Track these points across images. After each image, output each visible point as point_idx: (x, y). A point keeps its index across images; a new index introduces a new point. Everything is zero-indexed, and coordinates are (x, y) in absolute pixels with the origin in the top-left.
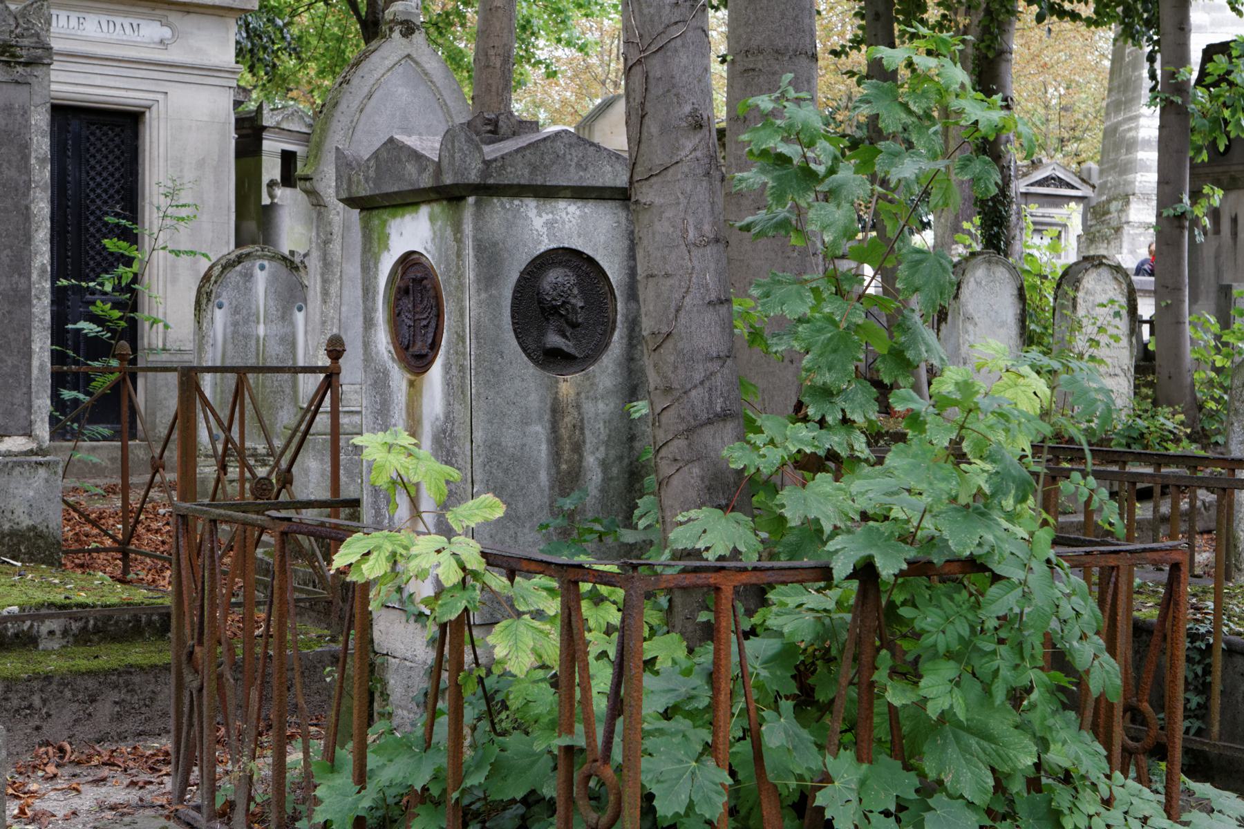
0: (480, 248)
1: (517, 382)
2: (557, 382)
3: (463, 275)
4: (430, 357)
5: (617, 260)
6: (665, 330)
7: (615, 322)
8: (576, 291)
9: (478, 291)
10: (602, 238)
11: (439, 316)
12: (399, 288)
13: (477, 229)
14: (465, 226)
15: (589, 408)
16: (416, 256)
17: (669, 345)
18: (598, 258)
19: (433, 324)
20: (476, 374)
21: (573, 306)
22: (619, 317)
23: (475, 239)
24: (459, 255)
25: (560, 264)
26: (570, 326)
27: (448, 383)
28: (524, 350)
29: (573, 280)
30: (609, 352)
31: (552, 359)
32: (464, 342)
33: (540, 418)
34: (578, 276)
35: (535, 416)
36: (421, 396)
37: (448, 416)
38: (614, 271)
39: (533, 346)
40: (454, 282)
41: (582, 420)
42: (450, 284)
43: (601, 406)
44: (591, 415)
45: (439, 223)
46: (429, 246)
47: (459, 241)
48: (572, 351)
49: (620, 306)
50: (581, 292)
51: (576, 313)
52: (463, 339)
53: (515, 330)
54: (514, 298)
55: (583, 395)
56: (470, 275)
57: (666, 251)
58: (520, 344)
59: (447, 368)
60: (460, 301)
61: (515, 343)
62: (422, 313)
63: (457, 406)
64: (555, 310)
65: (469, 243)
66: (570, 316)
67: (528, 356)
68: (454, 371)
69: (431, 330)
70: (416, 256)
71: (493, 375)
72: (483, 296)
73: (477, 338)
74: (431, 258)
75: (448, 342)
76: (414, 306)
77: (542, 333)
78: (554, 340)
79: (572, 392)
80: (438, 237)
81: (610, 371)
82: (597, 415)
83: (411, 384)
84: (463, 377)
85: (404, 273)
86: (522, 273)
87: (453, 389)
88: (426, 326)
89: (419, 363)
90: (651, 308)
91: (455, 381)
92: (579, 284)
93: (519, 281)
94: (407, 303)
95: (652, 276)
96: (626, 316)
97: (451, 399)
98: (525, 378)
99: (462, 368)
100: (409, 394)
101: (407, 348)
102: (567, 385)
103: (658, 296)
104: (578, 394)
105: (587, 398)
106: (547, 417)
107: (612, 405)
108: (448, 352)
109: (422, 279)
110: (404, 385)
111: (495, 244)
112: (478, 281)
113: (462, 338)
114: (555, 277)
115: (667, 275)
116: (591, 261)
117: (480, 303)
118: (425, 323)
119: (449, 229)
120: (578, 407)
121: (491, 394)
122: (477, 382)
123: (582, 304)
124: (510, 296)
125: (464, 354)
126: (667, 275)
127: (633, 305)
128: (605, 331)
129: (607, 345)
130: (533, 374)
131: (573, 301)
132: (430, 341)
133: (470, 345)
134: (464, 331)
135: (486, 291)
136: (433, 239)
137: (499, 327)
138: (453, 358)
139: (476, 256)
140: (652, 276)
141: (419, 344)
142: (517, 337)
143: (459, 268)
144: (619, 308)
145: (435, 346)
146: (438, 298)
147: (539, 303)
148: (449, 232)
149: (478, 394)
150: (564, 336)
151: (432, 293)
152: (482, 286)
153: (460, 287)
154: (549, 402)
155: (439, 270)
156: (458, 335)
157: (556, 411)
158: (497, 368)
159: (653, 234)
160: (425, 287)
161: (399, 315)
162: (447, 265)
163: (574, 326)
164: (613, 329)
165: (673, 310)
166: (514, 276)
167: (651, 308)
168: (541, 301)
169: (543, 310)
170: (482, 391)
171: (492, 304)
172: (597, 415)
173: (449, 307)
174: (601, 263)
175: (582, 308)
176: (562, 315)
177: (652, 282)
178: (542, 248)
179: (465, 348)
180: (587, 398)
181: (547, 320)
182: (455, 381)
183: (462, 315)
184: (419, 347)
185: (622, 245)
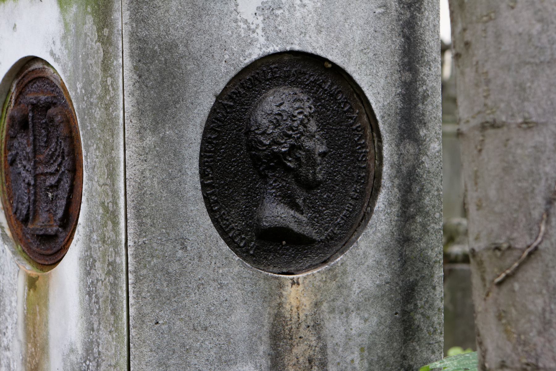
0: (143, 54)
1: (212, 291)
2: (281, 286)
3: (112, 102)
4: (61, 240)
5: (382, 71)
6: (522, 241)
7: (378, 176)
8: (313, 127)
9: (141, 133)
10: (358, 34)
11: (75, 170)
12: (12, 118)
13: (138, 19)
14: (117, 15)
15: (335, 328)
16: (37, 65)
17: (533, 273)
18: (350, 69)
19: (66, 185)
20: (138, 280)
21: (309, 153)
22: (386, 168)
23: (135, 38)
24: (106, 67)
25: (287, 80)
26: (300, 186)
27: (90, 291)
28: (223, 232)
29: (308, 106)
30: (369, 230)
31: (271, 248)
32: (116, 224)
33: (252, 351)
34: (317, 100)
35: (242, 348)
36: (46, 306)
37: (89, 347)
38: (378, 89)
39: (238, 225)
40: (98, 113)
41: (323, 350)
42: (92, 117)
43: (356, 322)
44: (339, 339)
45: (74, 9)
46: (58, 48)
47: (106, 41)
48: (307, 230)
49: (387, 150)
50: (322, 126)
51: (314, 165)
52: (113, 216)
53: (206, 198)
54: (206, 141)
55: (325, 306)
56: (125, 102)
57: (526, 72)
58: (215, 222)
59: (88, 265)
60: (108, 148)
61: (207, 221)
62: (48, 163)
63: (104, 335)
64: (278, 159)
65: (123, 45)
66: (303, 170)
67: (230, 242)
68: (99, 272)
69: (63, 193)
70: (37, 65)
71: (164, 279)
72: (150, 140)
73: (138, 216)
74: (61, 69)
75: (90, 220)
76: (35, 151)
77: (255, 201)
78: (276, 213)
79: (307, 302)
80: (72, 34)
81: (370, 262)
82: (349, 338)
83: (32, 283)
84: (115, 285)
85: (20, 93)
86: (219, 98)
87: (98, 304)
88: (55, 187)
89: (44, 249)
90: (492, 193)
91: (101, 290)
92: (319, 115)
93: (213, 111)
94: (24, 144)
95: (494, 125)
96: (397, 167)
97: (95, 319)
98: (228, 288)
99: (112, 269)
100: (28, 300)
101: (26, 221)
102: (299, 291)
103: (507, 170)
104: (317, 305)
105: (332, 311)
106: (263, 348)
107: (375, 320)
108: (89, 237)
109: (49, 105)
110: (21, 284)
111: (171, 47)
112: (140, 113)
113: (111, 215)
114: (277, 103)
115: (528, 125)
116: (338, 72)
117: (143, 154)
118: (52, 180)
119: (90, 20)
120: (317, 326)
121: (165, 315)
122: (138, 294)
123: (321, 149)
124: (199, 138)
125: (115, 244)
126: (528, 125)
127: (410, 148)
128: (362, 193)
129: (366, 217)
130: (239, 276)
131: (308, 144)
132: (60, 213)
133: (125, 229)
134: (115, 203)
135: (154, 131)
136: (64, 37)
137: (177, 194)
138: (98, 250)
139: (136, 68)
140: (494, 125)
141: (43, 217)
142: (210, 211)
143: (107, 91)
144: (386, 153)
145: (68, 222)
146: (72, 139)
147: (250, 148)
148: (90, 25)
149: (141, 316)
150: (294, 205)
151: (63, 131)
152: (147, 122)
153: (109, 124)
154: (267, 322)
155: (74, 91)
156: (106, 209)
157: (280, 337)
158: (174, 267)
159: (498, 36)
160: (52, 120)
161: (13, 162)
162: (88, 83)
163: (310, 186)
164: (376, 189)
165: (540, 200)
166: (207, 103)
167: (492, 193)
168: (252, 146)
169: (256, 161)
170: (147, 310)
171: (166, 153)
172: (349, 338)
173: (90, 157)
174: (356, 77)
175: (323, 155)
176: (288, 170)
177: (493, 139)
178: (255, 53)
179: (117, 234)
180: (332, 311)
181: (264, 177)
182: (101, 290)
183: (112, 174)
184: (44, 222)
185: (390, 46)
